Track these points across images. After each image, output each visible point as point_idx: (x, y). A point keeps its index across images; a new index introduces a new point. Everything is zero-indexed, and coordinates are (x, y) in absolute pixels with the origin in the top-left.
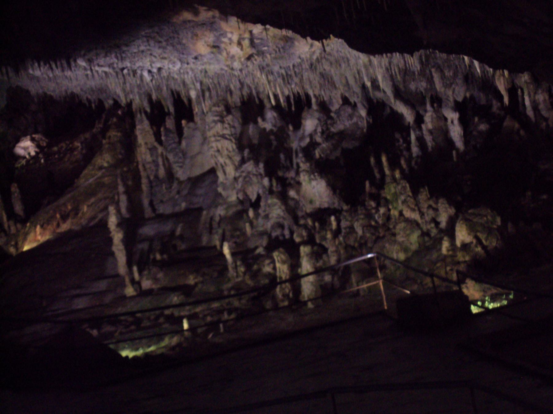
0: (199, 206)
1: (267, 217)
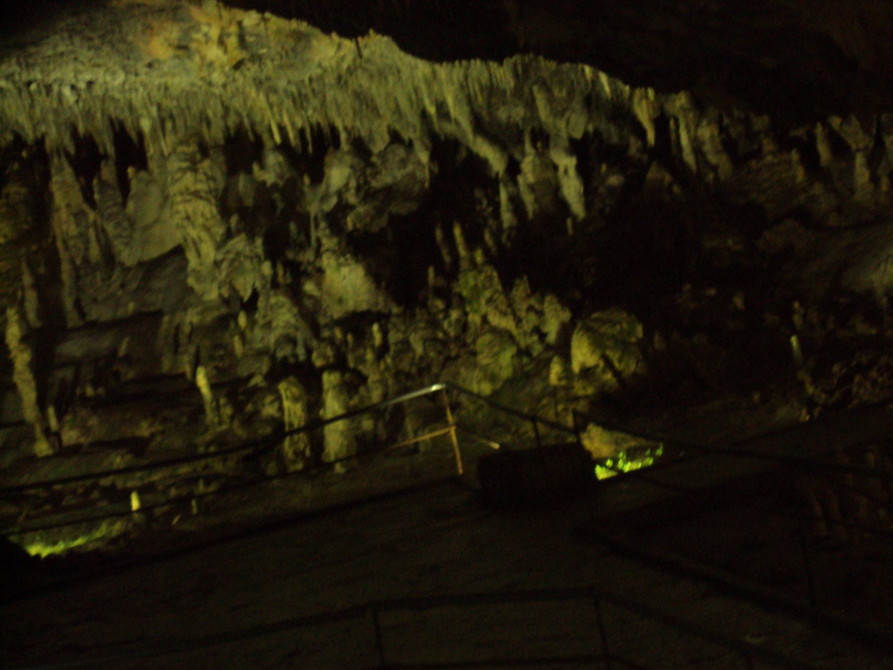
1: (268, 326)
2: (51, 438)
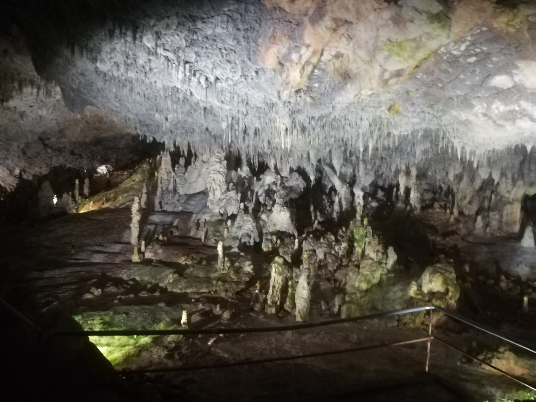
0: (190, 211)
1: (240, 227)
2: (140, 255)
